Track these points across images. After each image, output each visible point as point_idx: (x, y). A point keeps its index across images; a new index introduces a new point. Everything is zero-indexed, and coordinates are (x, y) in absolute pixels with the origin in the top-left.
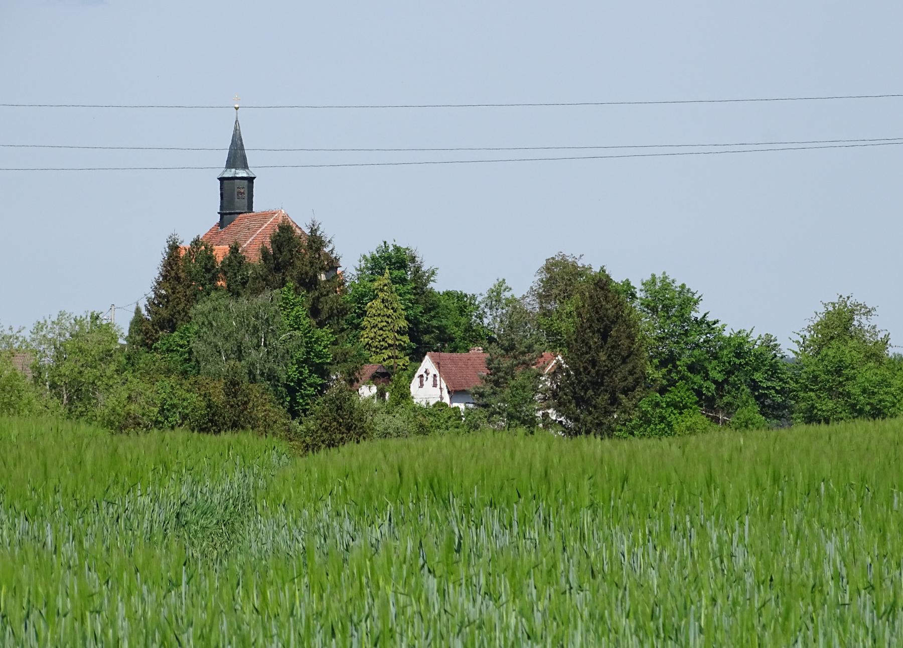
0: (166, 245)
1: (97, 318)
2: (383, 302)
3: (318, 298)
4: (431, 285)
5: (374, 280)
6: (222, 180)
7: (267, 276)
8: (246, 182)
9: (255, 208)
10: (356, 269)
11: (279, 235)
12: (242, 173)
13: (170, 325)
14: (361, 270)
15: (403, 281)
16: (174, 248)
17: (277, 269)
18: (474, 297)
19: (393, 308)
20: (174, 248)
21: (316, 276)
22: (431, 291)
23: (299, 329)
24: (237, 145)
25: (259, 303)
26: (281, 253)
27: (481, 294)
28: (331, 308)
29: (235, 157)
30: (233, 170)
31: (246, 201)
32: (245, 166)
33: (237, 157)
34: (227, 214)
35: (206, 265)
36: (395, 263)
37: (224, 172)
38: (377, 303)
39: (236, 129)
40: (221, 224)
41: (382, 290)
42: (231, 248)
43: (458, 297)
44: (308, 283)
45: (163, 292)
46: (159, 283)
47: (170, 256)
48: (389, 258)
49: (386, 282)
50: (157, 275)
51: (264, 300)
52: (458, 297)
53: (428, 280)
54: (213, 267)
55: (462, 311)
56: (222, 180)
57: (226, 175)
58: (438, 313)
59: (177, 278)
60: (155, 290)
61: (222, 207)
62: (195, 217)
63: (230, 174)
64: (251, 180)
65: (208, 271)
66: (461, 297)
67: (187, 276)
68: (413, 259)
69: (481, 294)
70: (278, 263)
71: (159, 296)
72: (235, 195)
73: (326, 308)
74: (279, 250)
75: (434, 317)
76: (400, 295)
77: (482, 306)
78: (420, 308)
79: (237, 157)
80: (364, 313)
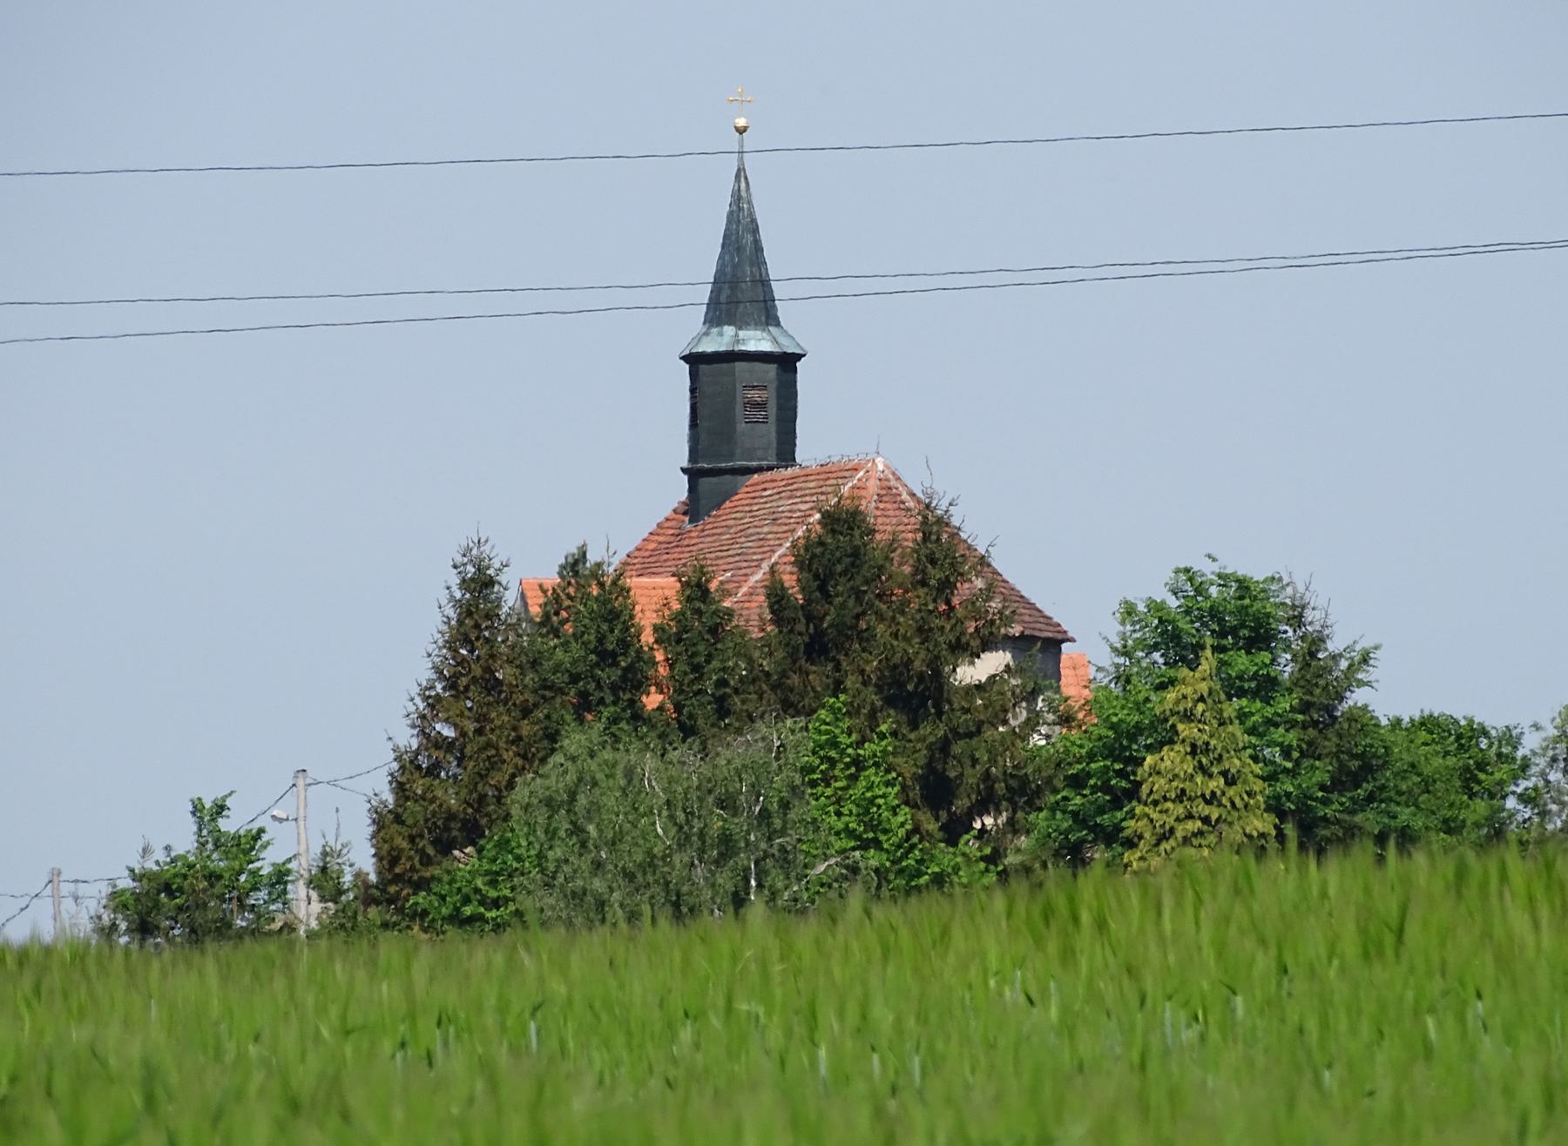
0: (455, 581)
1: (220, 809)
2: (1193, 753)
3: (944, 746)
4: (1357, 697)
5: (1172, 682)
6: (694, 360)
7: (784, 675)
8: (771, 370)
9: (810, 448)
10: (1114, 650)
11: (821, 543)
12: (756, 341)
13: (469, 828)
14: (1126, 653)
15: (1266, 687)
16: (480, 584)
17: (818, 648)
18: (1511, 738)
19: (1224, 774)
20: (480, 584)
21: (937, 674)
22: (1362, 721)
23: (877, 844)
24: (739, 250)
25: (737, 763)
26: (827, 596)
27: (1537, 727)
28: (987, 776)
29: (734, 283)
30: (729, 330)
31: (770, 430)
32: (768, 316)
33: (741, 287)
34: (713, 471)
35: (601, 639)
36: (1232, 632)
37: (698, 339)
38: (1172, 758)
39: (737, 198)
40: (694, 508)
41: (1188, 717)
42: (686, 585)
43: (1459, 737)
44: (917, 693)
45: (448, 732)
46: (434, 703)
47: (467, 611)
48: (1215, 613)
49: (1203, 688)
50: (425, 674)
51: (769, 745)
52: (1459, 737)
53: (1350, 679)
54: (624, 644)
55: (1469, 780)
56: (694, 360)
57: (708, 346)
58: (1383, 788)
59: (491, 685)
60: (422, 724)
61: (694, 454)
62: (590, 487)
63: (722, 340)
64: (787, 363)
65: (606, 657)
66: (1466, 736)
67: (528, 683)
68: (1297, 620)
69: (1537, 727)
70: (820, 634)
71: (434, 743)
72: (739, 409)
73: (972, 777)
74: (822, 588)
75: (1370, 798)
76: (1251, 731)
77: (1542, 762)
78: (1321, 772)
79: (741, 287)
80: (1133, 793)
